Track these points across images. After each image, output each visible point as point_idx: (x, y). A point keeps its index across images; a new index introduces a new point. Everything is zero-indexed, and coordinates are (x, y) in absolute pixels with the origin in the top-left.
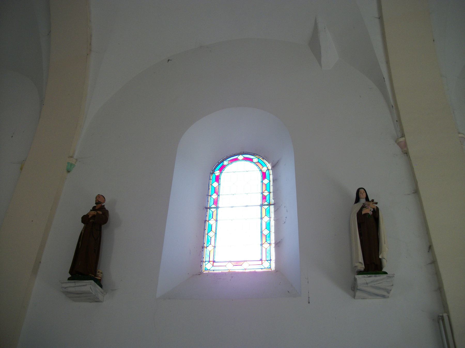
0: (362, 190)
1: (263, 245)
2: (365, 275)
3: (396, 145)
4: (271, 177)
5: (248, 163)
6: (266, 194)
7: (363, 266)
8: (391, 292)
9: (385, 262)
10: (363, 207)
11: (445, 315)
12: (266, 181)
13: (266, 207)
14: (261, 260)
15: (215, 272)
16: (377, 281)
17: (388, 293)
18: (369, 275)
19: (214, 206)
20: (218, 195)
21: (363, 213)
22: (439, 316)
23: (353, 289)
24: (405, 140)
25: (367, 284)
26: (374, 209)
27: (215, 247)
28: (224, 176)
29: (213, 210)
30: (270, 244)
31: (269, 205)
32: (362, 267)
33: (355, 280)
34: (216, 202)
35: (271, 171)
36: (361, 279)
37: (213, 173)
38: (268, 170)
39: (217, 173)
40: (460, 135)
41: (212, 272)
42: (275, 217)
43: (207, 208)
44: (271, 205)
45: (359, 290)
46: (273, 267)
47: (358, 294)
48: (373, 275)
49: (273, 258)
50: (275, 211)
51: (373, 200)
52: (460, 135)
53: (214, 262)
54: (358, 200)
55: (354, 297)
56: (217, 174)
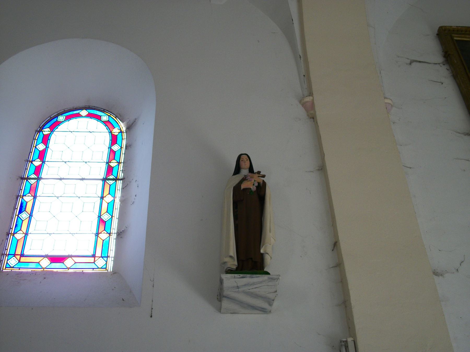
0: (244, 157)
1: (100, 235)
2: (236, 275)
3: (300, 106)
4: (124, 142)
5: (93, 121)
6: (113, 164)
7: (236, 263)
8: (275, 304)
9: (268, 259)
10: (244, 179)
11: (350, 340)
12: (115, 148)
13: (111, 182)
14: (94, 256)
15: (22, 270)
16: (254, 284)
17: (270, 305)
18: (241, 275)
19: (34, 176)
20: (43, 162)
21: (242, 188)
22: (341, 341)
23: (218, 297)
24: (313, 100)
25: (238, 287)
26: (259, 183)
27: (26, 234)
28: (57, 138)
29: (33, 182)
30: (110, 234)
31: (116, 179)
32: (233, 264)
33: (221, 281)
34: (38, 170)
35: (125, 135)
36: (230, 281)
37: (41, 130)
38: (121, 132)
39: (46, 131)
40: (387, 101)
41: (17, 270)
42: (122, 196)
43: (23, 179)
44: (119, 179)
45: (226, 297)
46: (110, 267)
47: (225, 304)
48: (248, 275)
49: (112, 254)
50: (123, 188)
51: (259, 172)
52: (387, 101)
53: (22, 255)
54: (237, 170)
55: (219, 310)
56: (45, 133)
